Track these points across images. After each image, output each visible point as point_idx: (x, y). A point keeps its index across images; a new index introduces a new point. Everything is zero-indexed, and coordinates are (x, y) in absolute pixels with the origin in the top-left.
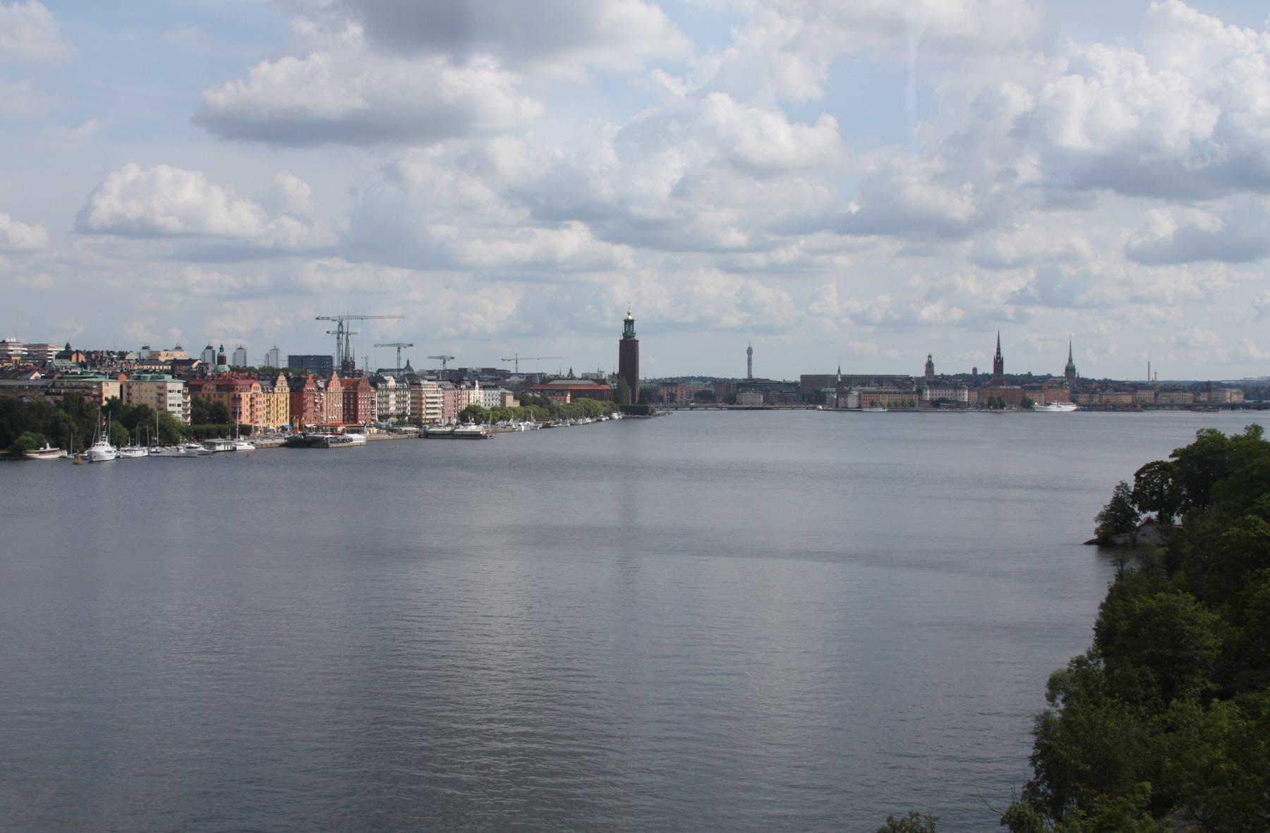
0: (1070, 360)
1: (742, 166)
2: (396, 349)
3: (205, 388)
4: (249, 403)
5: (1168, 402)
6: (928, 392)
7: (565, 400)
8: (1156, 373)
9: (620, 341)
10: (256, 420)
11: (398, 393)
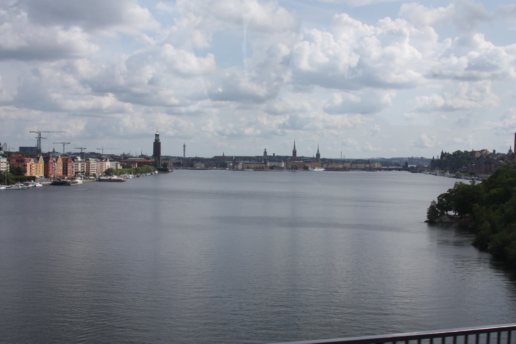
0: (318, 151)
1: (178, 73)
2: (63, 144)
3: (11, 161)
4: (30, 167)
5: (355, 167)
6: (269, 163)
7: (135, 166)
8: (344, 156)
9: (154, 142)
10: (32, 174)
11: (82, 163)
